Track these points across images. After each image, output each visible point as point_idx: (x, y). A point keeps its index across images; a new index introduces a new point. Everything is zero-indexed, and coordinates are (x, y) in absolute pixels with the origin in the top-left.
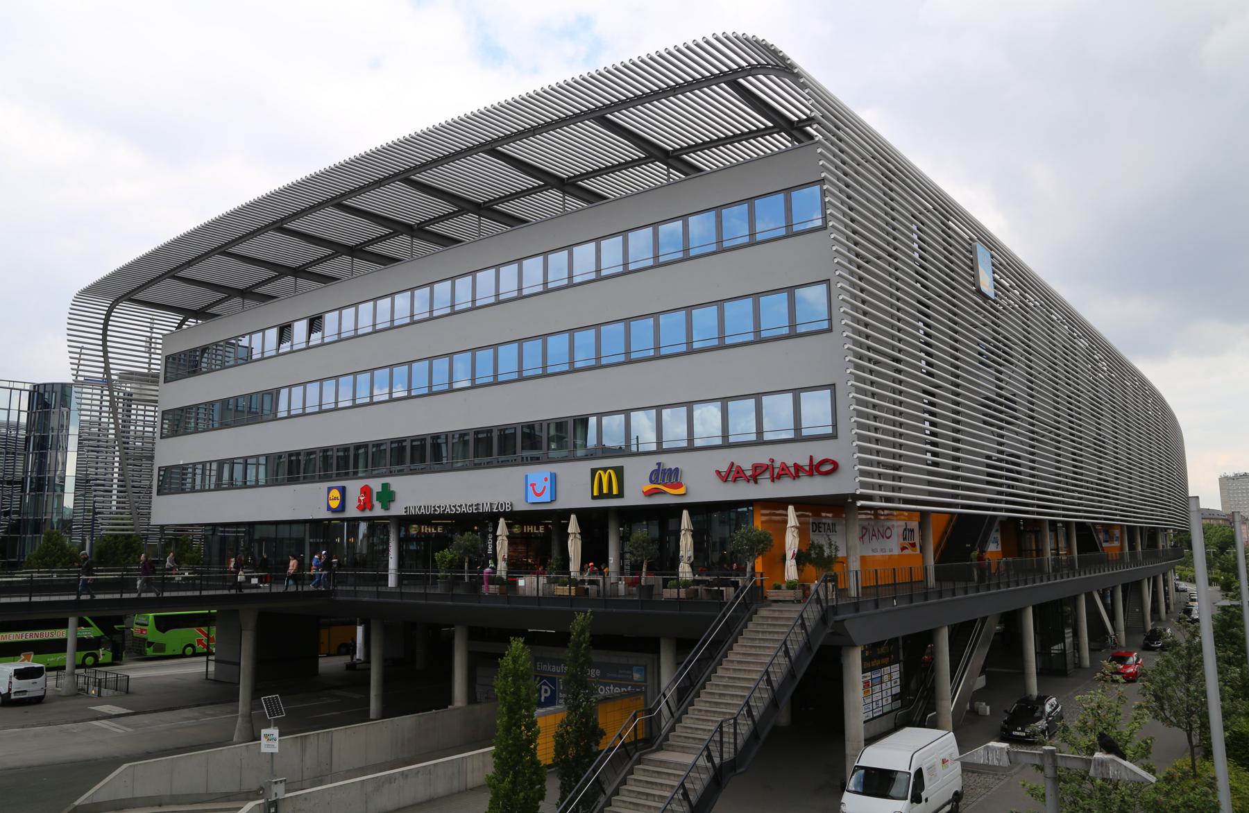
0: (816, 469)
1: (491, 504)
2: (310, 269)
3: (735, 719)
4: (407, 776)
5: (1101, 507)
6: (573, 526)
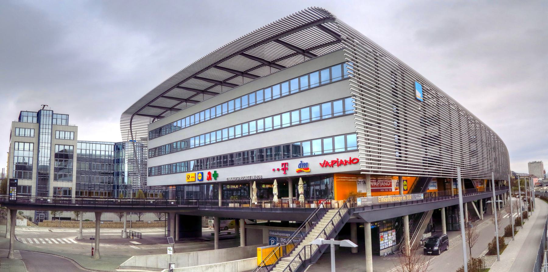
0: (352, 161)
1: (255, 176)
2: (208, 90)
5: (470, 173)
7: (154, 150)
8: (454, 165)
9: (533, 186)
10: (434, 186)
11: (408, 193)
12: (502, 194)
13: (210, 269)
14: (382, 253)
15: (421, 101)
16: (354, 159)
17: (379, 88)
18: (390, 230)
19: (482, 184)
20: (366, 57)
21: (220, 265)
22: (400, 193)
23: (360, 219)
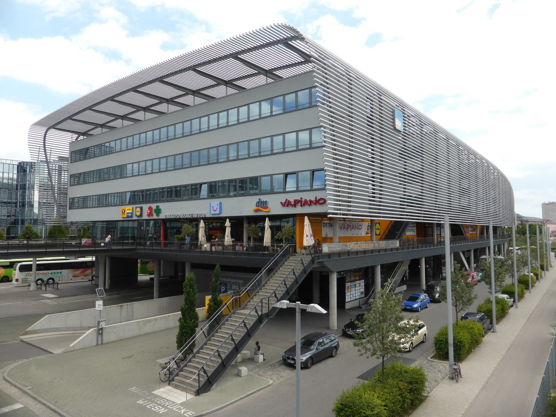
1: (197, 214)
2: (151, 108)
3: (269, 298)
4: (157, 320)
6: (228, 224)
7: (78, 175)
8: (439, 207)
10: (413, 231)
11: (381, 239)
12: (501, 244)
14: (348, 306)
19: (474, 230)
20: (339, 81)
21: (162, 318)
22: (371, 239)
23: (325, 267)
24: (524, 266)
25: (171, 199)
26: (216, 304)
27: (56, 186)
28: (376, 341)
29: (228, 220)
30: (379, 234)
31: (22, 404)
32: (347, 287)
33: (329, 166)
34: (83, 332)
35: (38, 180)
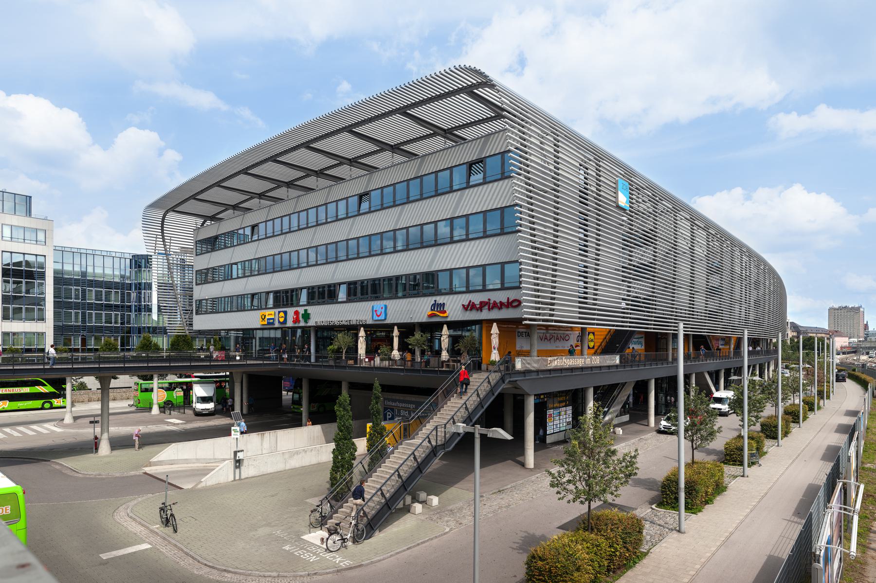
2: (295, 183)
5: (705, 326)
8: (676, 312)
9: (835, 352)
10: (640, 343)
11: (595, 354)
12: (765, 363)
13: (296, 456)
14: (549, 440)
15: (626, 210)
16: (515, 300)
17: (558, 192)
18: (563, 407)
24: (794, 393)
25: (323, 300)
26: (377, 435)
27: (179, 285)
28: (580, 481)
29: (396, 327)
30: (593, 348)
31: (150, 544)
32: (549, 415)
33: (525, 255)
34: (218, 464)
35: (156, 277)
